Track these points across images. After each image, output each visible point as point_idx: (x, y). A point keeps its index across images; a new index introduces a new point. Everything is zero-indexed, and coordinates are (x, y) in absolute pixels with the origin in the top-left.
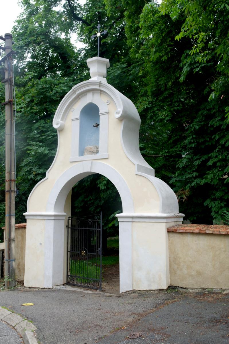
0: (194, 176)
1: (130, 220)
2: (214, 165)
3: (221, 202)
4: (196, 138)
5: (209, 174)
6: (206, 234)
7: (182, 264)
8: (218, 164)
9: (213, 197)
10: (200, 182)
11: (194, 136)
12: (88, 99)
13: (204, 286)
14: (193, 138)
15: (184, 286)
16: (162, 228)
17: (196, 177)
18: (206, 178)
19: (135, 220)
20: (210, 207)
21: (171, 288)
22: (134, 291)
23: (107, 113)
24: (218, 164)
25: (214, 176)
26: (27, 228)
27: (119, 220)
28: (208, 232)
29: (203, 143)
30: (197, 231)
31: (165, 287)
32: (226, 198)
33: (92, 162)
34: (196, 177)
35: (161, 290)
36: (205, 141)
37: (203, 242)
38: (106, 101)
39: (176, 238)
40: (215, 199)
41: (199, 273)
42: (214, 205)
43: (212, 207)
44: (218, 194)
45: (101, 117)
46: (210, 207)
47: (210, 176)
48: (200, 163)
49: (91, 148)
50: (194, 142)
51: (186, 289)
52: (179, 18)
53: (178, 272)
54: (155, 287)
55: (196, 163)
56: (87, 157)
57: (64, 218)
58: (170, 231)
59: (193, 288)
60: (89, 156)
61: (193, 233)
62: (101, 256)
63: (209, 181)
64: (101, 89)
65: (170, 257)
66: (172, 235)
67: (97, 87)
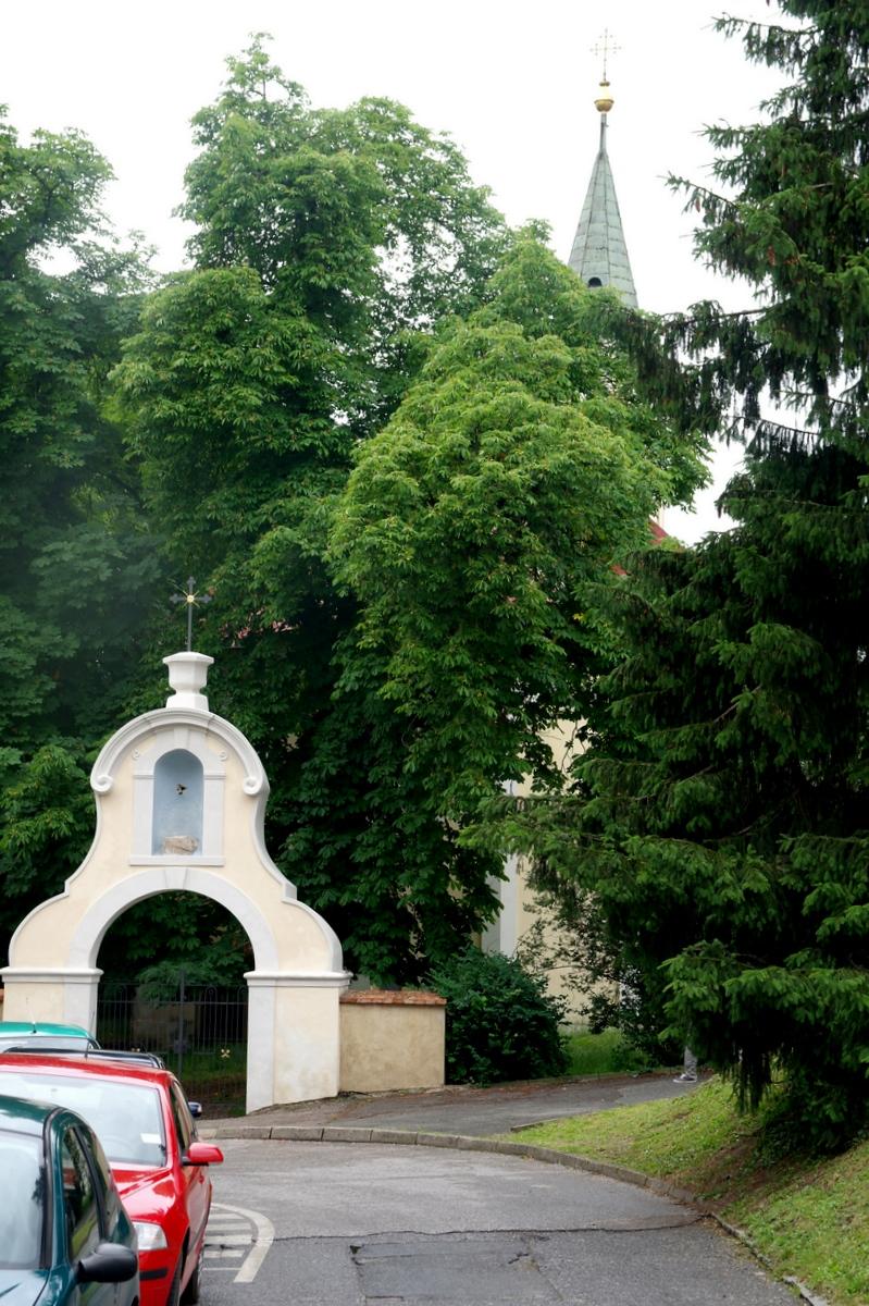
0: (323, 882)
1: (273, 983)
2: (370, 863)
3: (380, 945)
4: (329, 796)
5: (358, 882)
6: (403, 1005)
7: (362, 1054)
8: (380, 863)
9: (362, 932)
10: (338, 899)
11: (326, 791)
12: (178, 741)
13: (395, 1087)
14: (322, 795)
15: (364, 1091)
16: (333, 995)
17: (327, 886)
18: (354, 892)
19: (67, 980)
20: (356, 953)
21: (343, 1095)
22: (276, 1107)
23: (222, 778)
24: (380, 863)
25: (371, 889)
26: (337, 1001)
27: (249, 983)
28: (407, 1002)
29: (343, 807)
30: (389, 1001)
31: (335, 1094)
32: (393, 936)
33: (187, 871)
34: (327, 886)
35: (327, 1100)
36: (348, 803)
37: (397, 1017)
38: (220, 753)
39: (354, 1011)
40: (365, 938)
41: (389, 1067)
42: (364, 952)
43: (360, 954)
44: (377, 927)
45: (207, 783)
46: (356, 953)
47: (362, 888)
48: (334, 853)
49: (180, 841)
50: (324, 805)
51: (366, 1094)
52: (205, 263)
53: (355, 1068)
54: (317, 1095)
55: (326, 852)
56: (169, 858)
57: (89, 980)
58: (342, 1002)
59: (377, 1093)
60: (175, 856)
61: (382, 1005)
62: (180, 1057)
63: (358, 900)
64: (212, 728)
65: (341, 1046)
66: (345, 1008)
67: (205, 725)
